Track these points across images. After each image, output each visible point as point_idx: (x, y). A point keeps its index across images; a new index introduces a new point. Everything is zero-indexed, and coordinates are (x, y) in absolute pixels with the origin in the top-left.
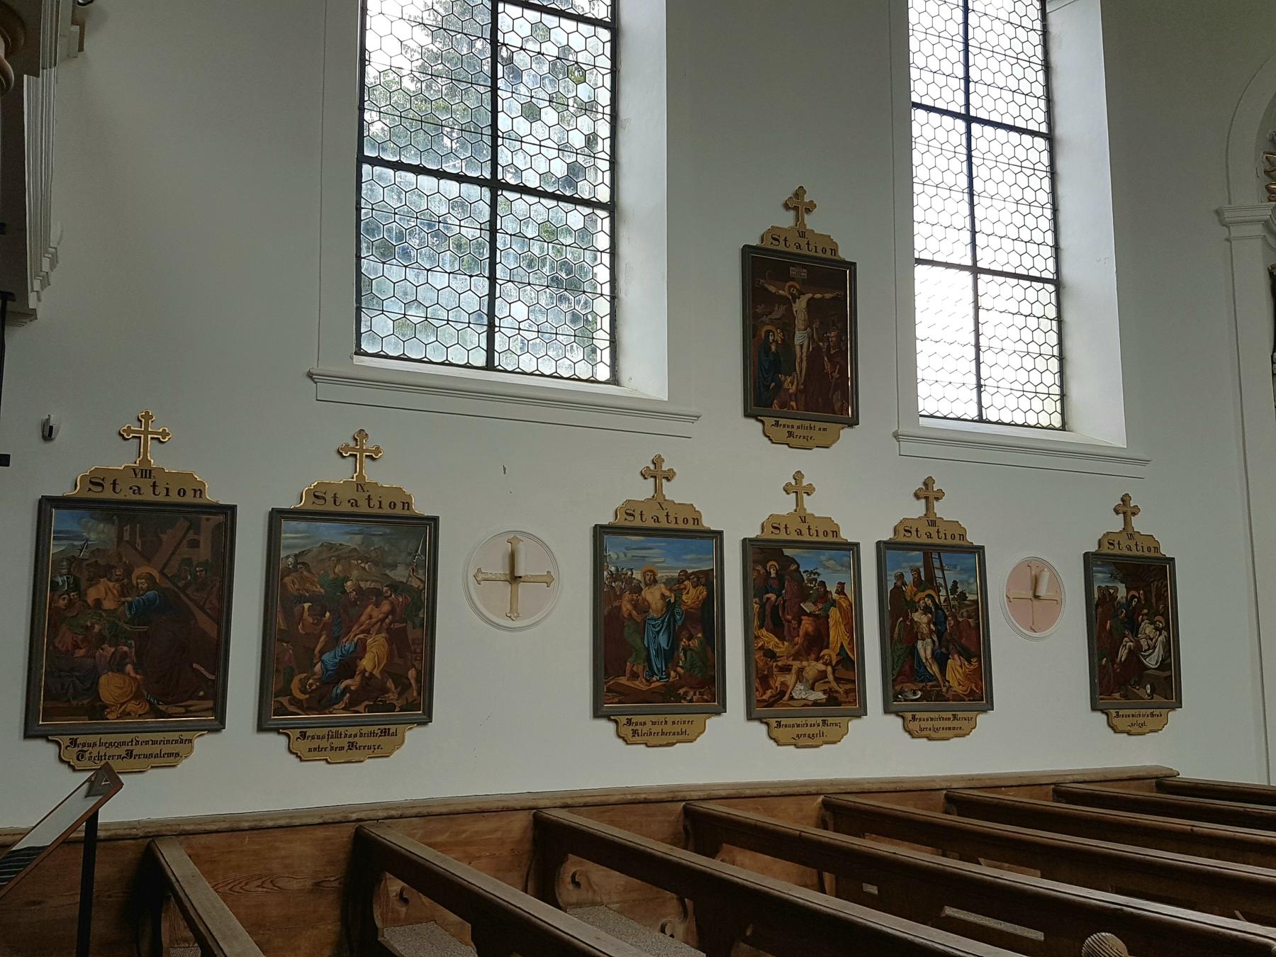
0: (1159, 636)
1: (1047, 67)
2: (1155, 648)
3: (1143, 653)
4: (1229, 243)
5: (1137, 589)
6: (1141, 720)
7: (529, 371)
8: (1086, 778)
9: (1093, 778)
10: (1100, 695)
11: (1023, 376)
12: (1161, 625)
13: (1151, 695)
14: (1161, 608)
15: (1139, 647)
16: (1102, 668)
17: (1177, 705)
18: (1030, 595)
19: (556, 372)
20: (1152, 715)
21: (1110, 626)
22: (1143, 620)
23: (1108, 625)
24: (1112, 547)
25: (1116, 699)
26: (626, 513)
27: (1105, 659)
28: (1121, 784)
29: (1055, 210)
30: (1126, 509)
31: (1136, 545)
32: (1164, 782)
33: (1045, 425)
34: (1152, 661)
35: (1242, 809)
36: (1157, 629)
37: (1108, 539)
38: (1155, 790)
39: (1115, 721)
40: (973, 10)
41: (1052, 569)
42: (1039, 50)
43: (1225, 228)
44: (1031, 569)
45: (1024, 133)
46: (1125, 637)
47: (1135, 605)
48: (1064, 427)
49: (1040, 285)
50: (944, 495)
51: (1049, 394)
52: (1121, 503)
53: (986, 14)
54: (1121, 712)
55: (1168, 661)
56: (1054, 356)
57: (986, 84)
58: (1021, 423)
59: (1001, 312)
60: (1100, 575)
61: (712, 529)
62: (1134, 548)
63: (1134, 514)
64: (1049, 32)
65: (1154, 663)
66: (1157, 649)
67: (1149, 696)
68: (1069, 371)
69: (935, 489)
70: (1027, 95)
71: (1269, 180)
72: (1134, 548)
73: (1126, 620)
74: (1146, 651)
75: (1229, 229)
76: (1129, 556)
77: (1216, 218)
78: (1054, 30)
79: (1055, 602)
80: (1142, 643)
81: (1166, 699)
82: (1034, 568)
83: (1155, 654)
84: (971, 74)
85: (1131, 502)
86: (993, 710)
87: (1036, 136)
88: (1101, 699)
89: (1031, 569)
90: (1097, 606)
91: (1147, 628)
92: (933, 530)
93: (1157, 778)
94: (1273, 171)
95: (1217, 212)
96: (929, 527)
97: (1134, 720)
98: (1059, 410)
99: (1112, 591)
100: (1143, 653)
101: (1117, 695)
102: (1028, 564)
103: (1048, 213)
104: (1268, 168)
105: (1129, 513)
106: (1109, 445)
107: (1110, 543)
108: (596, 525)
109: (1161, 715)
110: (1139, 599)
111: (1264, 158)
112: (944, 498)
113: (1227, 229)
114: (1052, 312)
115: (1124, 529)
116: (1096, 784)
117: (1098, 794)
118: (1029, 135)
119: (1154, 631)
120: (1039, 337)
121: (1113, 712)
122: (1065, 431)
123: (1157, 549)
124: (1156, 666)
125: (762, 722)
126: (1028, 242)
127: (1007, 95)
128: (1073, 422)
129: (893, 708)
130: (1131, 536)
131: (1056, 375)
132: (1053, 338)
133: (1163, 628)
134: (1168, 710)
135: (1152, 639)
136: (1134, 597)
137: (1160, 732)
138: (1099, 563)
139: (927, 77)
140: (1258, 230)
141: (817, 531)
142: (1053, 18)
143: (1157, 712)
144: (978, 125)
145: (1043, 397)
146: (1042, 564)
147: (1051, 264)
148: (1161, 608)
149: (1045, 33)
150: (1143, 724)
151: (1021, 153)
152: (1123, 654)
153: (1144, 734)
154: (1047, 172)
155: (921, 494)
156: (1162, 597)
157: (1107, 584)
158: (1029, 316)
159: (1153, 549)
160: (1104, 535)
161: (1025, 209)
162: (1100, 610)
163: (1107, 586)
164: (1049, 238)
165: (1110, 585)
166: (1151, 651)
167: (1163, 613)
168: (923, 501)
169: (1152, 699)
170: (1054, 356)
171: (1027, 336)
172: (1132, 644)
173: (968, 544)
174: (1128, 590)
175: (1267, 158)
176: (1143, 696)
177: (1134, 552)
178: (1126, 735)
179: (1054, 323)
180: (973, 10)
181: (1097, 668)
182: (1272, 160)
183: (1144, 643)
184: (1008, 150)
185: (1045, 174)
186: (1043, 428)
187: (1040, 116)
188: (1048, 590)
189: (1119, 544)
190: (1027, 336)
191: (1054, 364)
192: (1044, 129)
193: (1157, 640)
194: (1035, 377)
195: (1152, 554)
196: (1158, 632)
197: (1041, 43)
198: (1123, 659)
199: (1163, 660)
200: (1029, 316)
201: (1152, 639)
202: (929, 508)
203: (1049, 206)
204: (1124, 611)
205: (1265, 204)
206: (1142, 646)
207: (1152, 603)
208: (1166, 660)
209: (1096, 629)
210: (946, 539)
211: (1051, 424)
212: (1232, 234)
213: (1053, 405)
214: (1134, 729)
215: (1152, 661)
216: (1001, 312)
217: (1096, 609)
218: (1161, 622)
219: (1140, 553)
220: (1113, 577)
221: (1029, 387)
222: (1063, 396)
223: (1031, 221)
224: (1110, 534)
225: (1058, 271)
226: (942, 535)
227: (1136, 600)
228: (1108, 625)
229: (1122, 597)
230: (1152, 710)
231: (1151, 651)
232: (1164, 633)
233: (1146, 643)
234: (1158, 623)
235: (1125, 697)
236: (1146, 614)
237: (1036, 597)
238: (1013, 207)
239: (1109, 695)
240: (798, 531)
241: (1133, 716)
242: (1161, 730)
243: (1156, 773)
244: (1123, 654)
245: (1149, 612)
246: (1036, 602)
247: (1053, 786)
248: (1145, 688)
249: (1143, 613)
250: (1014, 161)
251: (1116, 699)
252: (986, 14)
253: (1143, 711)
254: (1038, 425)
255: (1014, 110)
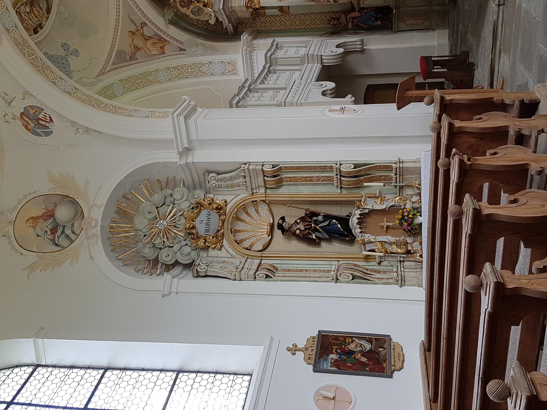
0: (355, 341)
1: (72, 367)
2: (361, 344)
3: (364, 350)
4: (178, 293)
5: (332, 349)
6: (397, 355)
7: (247, 390)
8: (427, 385)
9: (426, 381)
10: (384, 373)
11: (222, 393)
12: (350, 340)
13: (385, 349)
14: (342, 339)
15: (361, 351)
16: (371, 370)
17: (389, 337)
18: (333, 401)
19: (245, 393)
20: (394, 349)
21: (350, 364)
22: (348, 348)
23: (350, 365)
24: (311, 358)
25: (386, 366)
26: (309, 360)
27: (366, 368)
28: (428, 367)
29: (143, 370)
30: (294, 350)
31: (311, 347)
32: (427, 348)
33: (248, 384)
34: (368, 346)
35: (435, 315)
36: (352, 342)
37: (307, 360)
38: (430, 352)
39: (398, 367)
40: (31, 401)
41: (321, 389)
42: (62, 370)
43: (171, 294)
44: (319, 400)
45: (101, 382)
46: (355, 357)
47: (340, 351)
48: (251, 375)
49: (178, 380)
50: (295, 344)
51: (233, 380)
52: (290, 351)
53: (35, 395)
54: (393, 364)
55: (368, 339)
56: (215, 377)
57: (84, 374)
58: (245, 396)
59: (187, 401)
60: (325, 366)
61: (317, 333)
62: (312, 348)
63: (296, 346)
64: (55, 364)
65: (369, 345)
66: (362, 343)
67: (385, 350)
68: (223, 370)
69: (292, 347)
70: (82, 378)
71: (155, 274)
72: (312, 348)
73: (347, 356)
74: (363, 348)
75: (172, 292)
76: (316, 351)
77: (166, 297)
78: (54, 363)
79: (337, 389)
80: (358, 350)
81: (386, 342)
82: (319, 398)
83: (364, 344)
84: (63, 406)
85: (290, 347)
86: (390, 335)
87: (104, 376)
88: (386, 373)
89: (319, 400)
90: (340, 369)
91: (352, 347)
92: (310, 349)
93: (425, 351)
94: (151, 272)
95: (163, 297)
96: (309, 350)
97: (397, 359)
98: (242, 376)
99: (333, 361)
100: (364, 350)
101: (384, 365)
102: (317, 401)
103: (144, 373)
104: (149, 274)
105: (296, 348)
106: (262, 355)
107: (309, 359)
108: (313, 371)
109: (394, 345)
110: (337, 349)
111: (144, 275)
112: (296, 344)
113: (172, 293)
114: (193, 375)
115: (303, 352)
116: (429, 381)
117: (434, 381)
118: (102, 379)
119: (353, 343)
120: (204, 383)
121: (393, 368)
122: (252, 374)
123: (314, 338)
124: (370, 344)
125: (393, 373)
126: (158, 378)
127: (80, 387)
128: (249, 371)
129: (390, 374)
130: (307, 349)
131: (224, 376)
132: (206, 376)
133: (352, 339)
134: (391, 342)
135: (357, 345)
136: (336, 351)
137: (402, 346)
138: (318, 365)
139: (73, 400)
140: (175, 280)
141: (312, 344)
142: (49, 363)
143: (392, 347)
144: (100, 385)
145: (234, 383)
146: (317, 393)
147: (169, 374)
148: (342, 339)
149: (55, 366)
150: (399, 354)
151: (110, 384)
152: (364, 359)
153: (404, 354)
154: (123, 372)
155: (293, 352)
156: (336, 338)
157: (329, 363)
158: (192, 387)
159: (314, 340)
160: (305, 361)
161: (139, 384)
162: (342, 368)
163: (330, 363)
164: (156, 373)
165: (330, 362)
166: (363, 346)
167: (344, 338)
168: (296, 352)
169: (386, 348)
170: (215, 377)
171: (202, 389)
172: (359, 355)
173: (317, 336)
174: (332, 353)
175: (144, 274)
176: (385, 352)
177: (315, 348)
178: (404, 363)
179: (199, 374)
180: (31, 401)
181: (371, 373)
182: (146, 272)
183: (358, 349)
184: (107, 390)
185: (124, 373)
186: (249, 385)
187: (95, 372)
188: (331, 392)
189: (310, 355)
190: (202, 389)
191: (219, 377)
192: (101, 371)
193: (357, 343)
194: (223, 386)
195: (316, 340)
196: (354, 342)
197: (59, 368)
198: (366, 360)
199: (367, 341)
200: (192, 387)
201: (357, 345)
202: (300, 350)
203: (140, 372)
204: (343, 356)
205: (164, 276)
206: (360, 350)
207: (339, 343)
208: (367, 340)
209: (350, 371)
210: (314, 344)
211: (248, 381)
212: (175, 291)
213: (239, 379)
214: (401, 359)
215: (368, 346)
216: (187, 401)
217: (341, 369)
218: (349, 340)
219: (315, 346)
220: (326, 359)
221: (228, 390)
222: (235, 374)
223: (145, 382)
224: (305, 358)
225: (173, 371)
226: (312, 345)
227: (337, 350)
228: (350, 365)
229: (336, 356)
230: (392, 349)
231: (363, 346)
232: (354, 339)
233: (359, 348)
234: (349, 341)
235: (385, 361)
236: (345, 346)
237: (334, 398)
238: (136, 390)
239: (384, 369)
240: (311, 351)
241: (394, 358)
242: (401, 346)
243: (422, 351)
244: (364, 359)
245: (343, 345)
246: (336, 399)
247: (432, 403)
248: (381, 351)
249: (344, 348)
250: (113, 388)
251: (386, 366)
252: (35, 395)
253: (392, 353)
254: (248, 387)
255: (89, 385)
